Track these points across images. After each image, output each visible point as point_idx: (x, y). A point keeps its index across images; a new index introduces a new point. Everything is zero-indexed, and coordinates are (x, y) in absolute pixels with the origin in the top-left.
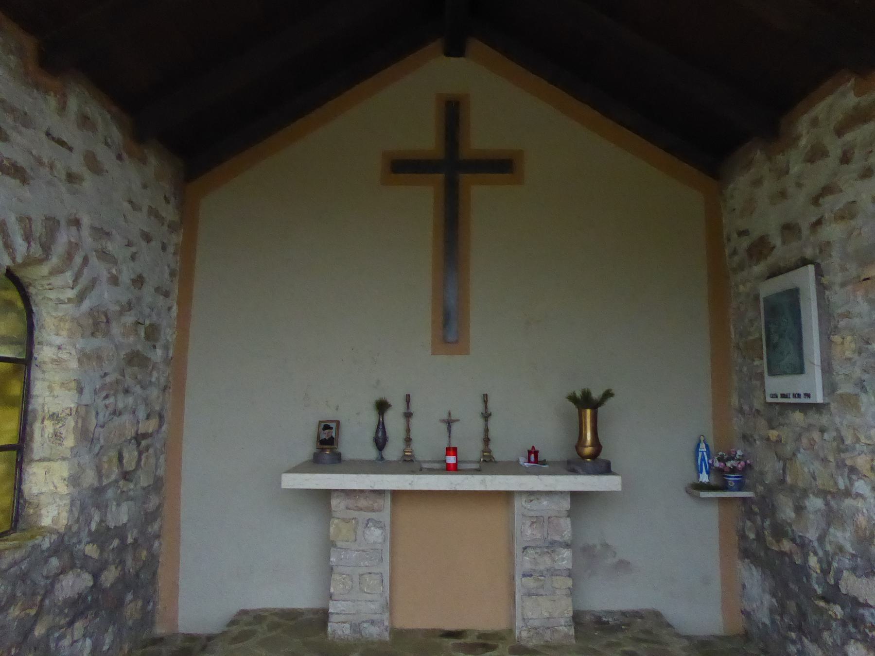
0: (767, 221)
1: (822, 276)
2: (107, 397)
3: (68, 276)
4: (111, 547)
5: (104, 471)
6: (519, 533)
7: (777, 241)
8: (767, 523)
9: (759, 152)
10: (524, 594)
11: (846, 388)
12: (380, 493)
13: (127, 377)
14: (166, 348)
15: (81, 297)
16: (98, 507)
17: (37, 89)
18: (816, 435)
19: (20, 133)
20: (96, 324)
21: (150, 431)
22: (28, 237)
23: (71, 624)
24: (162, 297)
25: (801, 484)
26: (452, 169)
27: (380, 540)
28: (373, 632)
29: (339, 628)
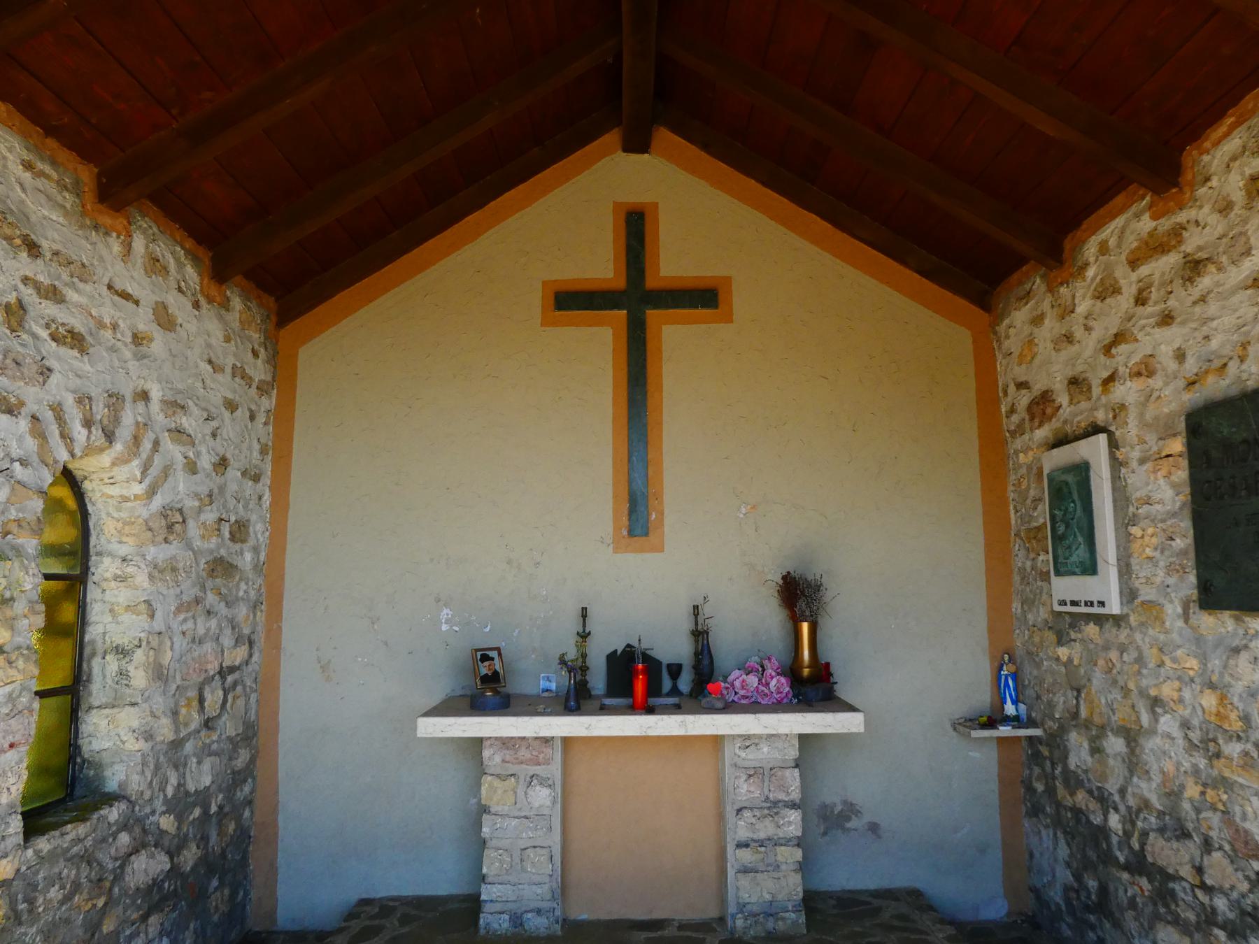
0: (1051, 373)
1: (1118, 449)
2: (185, 620)
3: (135, 466)
4: (191, 818)
5: (181, 718)
6: (731, 789)
7: (1063, 399)
8: (1058, 771)
9: (1038, 281)
10: (739, 872)
11: (1147, 594)
12: (547, 741)
13: (209, 593)
14: (256, 550)
15: (152, 492)
16: (176, 767)
17: (97, 231)
18: (1114, 655)
19: (77, 290)
20: (170, 527)
21: (237, 663)
22: (88, 424)
23: (144, 918)
24: (250, 483)
25: (1097, 720)
26: (636, 300)
27: (548, 803)
28: (537, 924)
29: (493, 920)
